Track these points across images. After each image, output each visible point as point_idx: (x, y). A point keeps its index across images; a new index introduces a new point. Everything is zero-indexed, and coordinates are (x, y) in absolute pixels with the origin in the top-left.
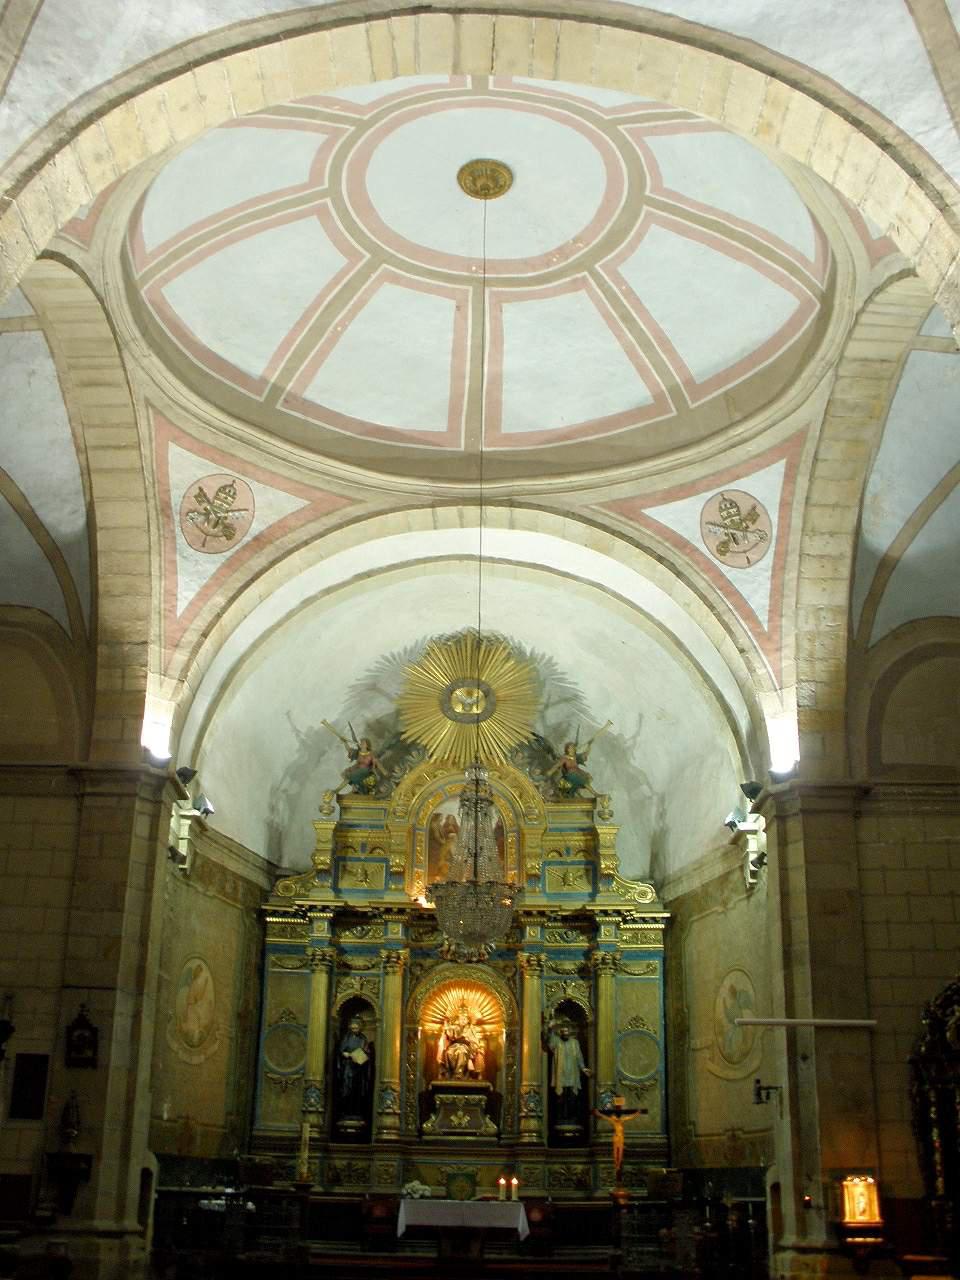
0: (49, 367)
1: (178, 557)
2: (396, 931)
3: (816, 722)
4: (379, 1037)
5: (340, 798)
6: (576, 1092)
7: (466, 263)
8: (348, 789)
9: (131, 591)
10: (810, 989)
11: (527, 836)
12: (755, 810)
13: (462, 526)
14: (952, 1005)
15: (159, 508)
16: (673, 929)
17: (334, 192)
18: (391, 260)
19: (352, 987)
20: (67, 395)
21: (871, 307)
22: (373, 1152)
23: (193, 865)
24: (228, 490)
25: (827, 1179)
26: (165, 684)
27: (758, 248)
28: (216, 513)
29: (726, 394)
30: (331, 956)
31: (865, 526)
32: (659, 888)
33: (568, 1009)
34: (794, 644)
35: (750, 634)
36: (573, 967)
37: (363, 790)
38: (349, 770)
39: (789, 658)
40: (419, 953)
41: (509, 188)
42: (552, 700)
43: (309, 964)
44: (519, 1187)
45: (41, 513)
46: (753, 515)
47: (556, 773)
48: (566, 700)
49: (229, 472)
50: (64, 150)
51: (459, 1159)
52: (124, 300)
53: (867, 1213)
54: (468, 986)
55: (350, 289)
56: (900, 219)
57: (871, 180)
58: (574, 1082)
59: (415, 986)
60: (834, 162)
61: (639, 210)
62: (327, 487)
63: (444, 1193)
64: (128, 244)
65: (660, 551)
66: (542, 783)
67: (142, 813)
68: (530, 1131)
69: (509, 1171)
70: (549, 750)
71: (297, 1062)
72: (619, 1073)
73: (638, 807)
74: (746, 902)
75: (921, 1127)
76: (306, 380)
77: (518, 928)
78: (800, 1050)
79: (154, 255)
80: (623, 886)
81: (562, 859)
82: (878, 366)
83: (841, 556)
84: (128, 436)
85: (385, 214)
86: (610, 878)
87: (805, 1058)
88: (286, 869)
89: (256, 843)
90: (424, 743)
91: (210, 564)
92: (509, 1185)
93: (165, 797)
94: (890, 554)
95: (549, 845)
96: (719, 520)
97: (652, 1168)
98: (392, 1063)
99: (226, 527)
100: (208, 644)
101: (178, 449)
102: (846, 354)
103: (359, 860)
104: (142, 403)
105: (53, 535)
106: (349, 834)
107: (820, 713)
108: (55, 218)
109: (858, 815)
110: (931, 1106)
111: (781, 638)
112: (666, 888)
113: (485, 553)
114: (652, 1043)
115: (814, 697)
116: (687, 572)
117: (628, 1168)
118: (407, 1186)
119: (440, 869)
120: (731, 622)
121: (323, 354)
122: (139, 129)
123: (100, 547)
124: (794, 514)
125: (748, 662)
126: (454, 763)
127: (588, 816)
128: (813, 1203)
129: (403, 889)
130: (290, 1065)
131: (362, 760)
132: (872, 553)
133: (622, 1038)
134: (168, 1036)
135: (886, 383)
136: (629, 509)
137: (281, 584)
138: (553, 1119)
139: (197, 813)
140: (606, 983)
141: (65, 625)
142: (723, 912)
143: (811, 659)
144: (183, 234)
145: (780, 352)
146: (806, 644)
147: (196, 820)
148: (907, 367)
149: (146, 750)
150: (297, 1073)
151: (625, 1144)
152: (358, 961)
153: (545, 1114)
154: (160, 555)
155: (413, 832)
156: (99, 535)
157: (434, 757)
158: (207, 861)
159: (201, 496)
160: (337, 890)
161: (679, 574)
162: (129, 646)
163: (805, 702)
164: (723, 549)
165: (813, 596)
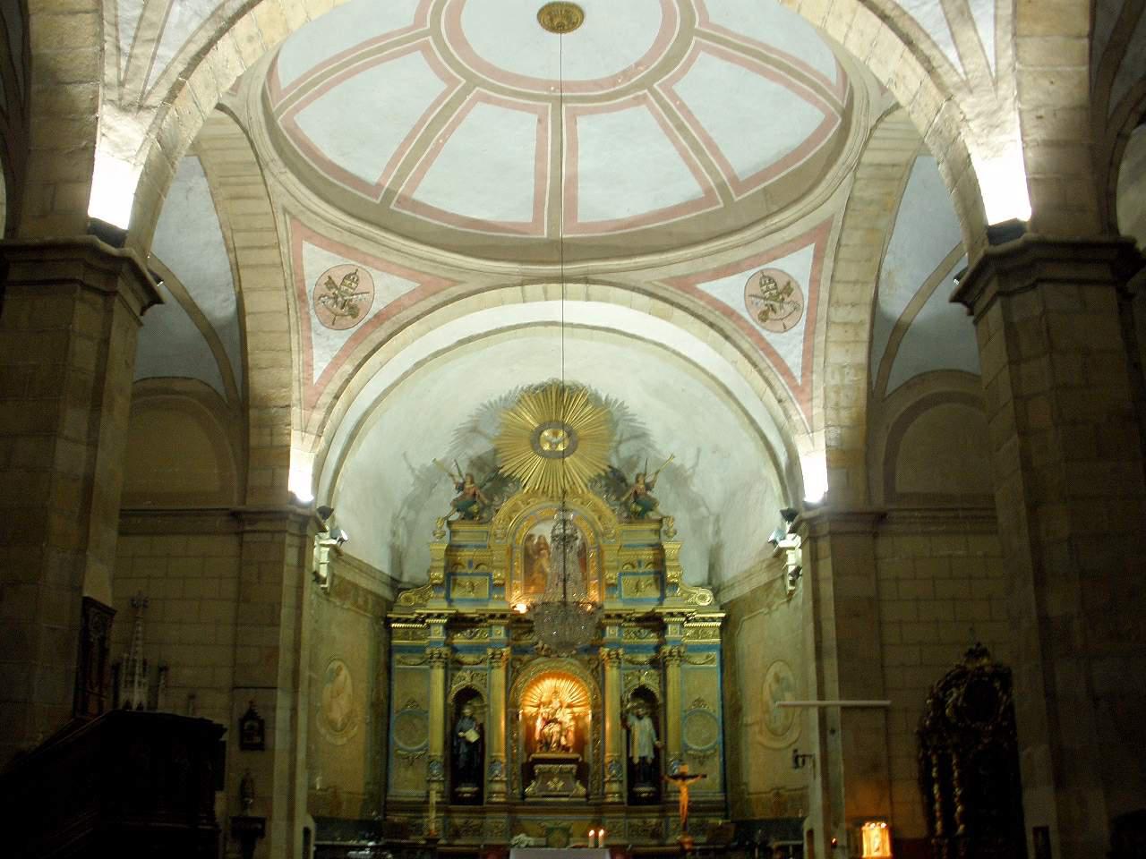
0: (202, 184)
1: (313, 335)
2: (500, 633)
3: (840, 459)
4: (487, 718)
5: (449, 524)
6: (649, 761)
7: (547, 84)
8: (456, 516)
9: (275, 364)
10: (837, 677)
11: (606, 553)
12: (793, 531)
13: (547, 300)
14: (951, 688)
15: (296, 295)
16: (728, 627)
17: (436, 31)
18: (484, 84)
19: (464, 679)
20: (218, 206)
21: (882, 125)
22: (484, 812)
23: (331, 584)
24: (352, 277)
25: (851, 826)
26: (306, 440)
27: (790, 71)
28: (343, 297)
29: (765, 189)
30: (446, 655)
31: (881, 298)
32: (716, 592)
33: (642, 693)
34: (822, 396)
35: (787, 387)
36: (645, 659)
37: (468, 516)
38: (455, 500)
39: (819, 407)
40: (519, 651)
41: (581, 23)
42: (624, 437)
43: (428, 661)
44: (605, 837)
45: (198, 302)
46: (788, 289)
47: (628, 498)
48: (636, 437)
49: (353, 262)
50: (223, 37)
51: (558, 816)
52: (264, 130)
53: (881, 850)
54: (559, 676)
55: (450, 107)
56: (897, 75)
57: (874, 44)
58: (648, 753)
59: (516, 678)
60: (845, 29)
61: (691, 39)
62: (435, 272)
63: (544, 844)
64: (267, 87)
65: (711, 318)
66: (617, 508)
67: (290, 546)
68: (614, 793)
69: (597, 825)
70: (623, 480)
71: (421, 742)
72: (686, 746)
73: (698, 525)
74: (786, 605)
75: (925, 783)
76: (414, 184)
77: (601, 628)
78: (830, 725)
79: (287, 91)
80: (685, 592)
81: (635, 570)
82: (889, 170)
83: (862, 323)
84: (269, 238)
85: (478, 49)
86: (675, 585)
87: (833, 732)
88: (405, 583)
89: (380, 562)
90: (518, 476)
91: (339, 339)
92: (596, 835)
93: (309, 532)
94: (903, 319)
95: (624, 559)
96: (760, 294)
97: (712, 821)
98: (499, 739)
99: (352, 308)
100: (339, 405)
101: (311, 246)
102: (863, 160)
103: (466, 574)
104: (280, 211)
105: (209, 319)
106: (459, 553)
107: (844, 452)
108: (217, 89)
109: (875, 536)
110: (932, 767)
111: (812, 391)
112: (721, 593)
113: (567, 320)
114: (712, 720)
115: (840, 439)
116: (735, 336)
117: (694, 820)
118: (516, 838)
119: (534, 580)
120: (771, 377)
121: (428, 162)
122: (281, 14)
123: (249, 329)
124: (822, 288)
125: (785, 411)
126: (543, 492)
127: (655, 534)
128: (839, 844)
129: (504, 598)
130: (415, 744)
131: (467, 491)
132: (887, 320)
133: (687, 717)
134: (318, 724)
135: (896, 183)
136: (685, 284)
137: (396, 353)
138: (631, 783)
139: (334, 542)
140: (673, 671)
141: (221, 390)
142: (768, 613)
143: (837, 407)
144: (311, 73)
145: (808, 157)
146: (832, 395)
147: (334, 548)
148: (914, 169)
149: (292, 495)
150: (421, 749)
151: (689, 802)
152: (469, 658)
153: (625, 779)
154: (298, 334)
155: (511, 551)
156: (247, 319)
157: (527, 488)
158: (343, 580)
159: (330, 283)
160: (450, 601)
161: (727, 337)
162: (275, 409)
163: (833, 443)
164: (763, 317)
165: (838, 356)
